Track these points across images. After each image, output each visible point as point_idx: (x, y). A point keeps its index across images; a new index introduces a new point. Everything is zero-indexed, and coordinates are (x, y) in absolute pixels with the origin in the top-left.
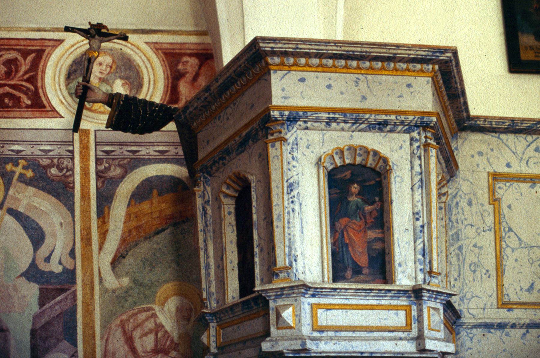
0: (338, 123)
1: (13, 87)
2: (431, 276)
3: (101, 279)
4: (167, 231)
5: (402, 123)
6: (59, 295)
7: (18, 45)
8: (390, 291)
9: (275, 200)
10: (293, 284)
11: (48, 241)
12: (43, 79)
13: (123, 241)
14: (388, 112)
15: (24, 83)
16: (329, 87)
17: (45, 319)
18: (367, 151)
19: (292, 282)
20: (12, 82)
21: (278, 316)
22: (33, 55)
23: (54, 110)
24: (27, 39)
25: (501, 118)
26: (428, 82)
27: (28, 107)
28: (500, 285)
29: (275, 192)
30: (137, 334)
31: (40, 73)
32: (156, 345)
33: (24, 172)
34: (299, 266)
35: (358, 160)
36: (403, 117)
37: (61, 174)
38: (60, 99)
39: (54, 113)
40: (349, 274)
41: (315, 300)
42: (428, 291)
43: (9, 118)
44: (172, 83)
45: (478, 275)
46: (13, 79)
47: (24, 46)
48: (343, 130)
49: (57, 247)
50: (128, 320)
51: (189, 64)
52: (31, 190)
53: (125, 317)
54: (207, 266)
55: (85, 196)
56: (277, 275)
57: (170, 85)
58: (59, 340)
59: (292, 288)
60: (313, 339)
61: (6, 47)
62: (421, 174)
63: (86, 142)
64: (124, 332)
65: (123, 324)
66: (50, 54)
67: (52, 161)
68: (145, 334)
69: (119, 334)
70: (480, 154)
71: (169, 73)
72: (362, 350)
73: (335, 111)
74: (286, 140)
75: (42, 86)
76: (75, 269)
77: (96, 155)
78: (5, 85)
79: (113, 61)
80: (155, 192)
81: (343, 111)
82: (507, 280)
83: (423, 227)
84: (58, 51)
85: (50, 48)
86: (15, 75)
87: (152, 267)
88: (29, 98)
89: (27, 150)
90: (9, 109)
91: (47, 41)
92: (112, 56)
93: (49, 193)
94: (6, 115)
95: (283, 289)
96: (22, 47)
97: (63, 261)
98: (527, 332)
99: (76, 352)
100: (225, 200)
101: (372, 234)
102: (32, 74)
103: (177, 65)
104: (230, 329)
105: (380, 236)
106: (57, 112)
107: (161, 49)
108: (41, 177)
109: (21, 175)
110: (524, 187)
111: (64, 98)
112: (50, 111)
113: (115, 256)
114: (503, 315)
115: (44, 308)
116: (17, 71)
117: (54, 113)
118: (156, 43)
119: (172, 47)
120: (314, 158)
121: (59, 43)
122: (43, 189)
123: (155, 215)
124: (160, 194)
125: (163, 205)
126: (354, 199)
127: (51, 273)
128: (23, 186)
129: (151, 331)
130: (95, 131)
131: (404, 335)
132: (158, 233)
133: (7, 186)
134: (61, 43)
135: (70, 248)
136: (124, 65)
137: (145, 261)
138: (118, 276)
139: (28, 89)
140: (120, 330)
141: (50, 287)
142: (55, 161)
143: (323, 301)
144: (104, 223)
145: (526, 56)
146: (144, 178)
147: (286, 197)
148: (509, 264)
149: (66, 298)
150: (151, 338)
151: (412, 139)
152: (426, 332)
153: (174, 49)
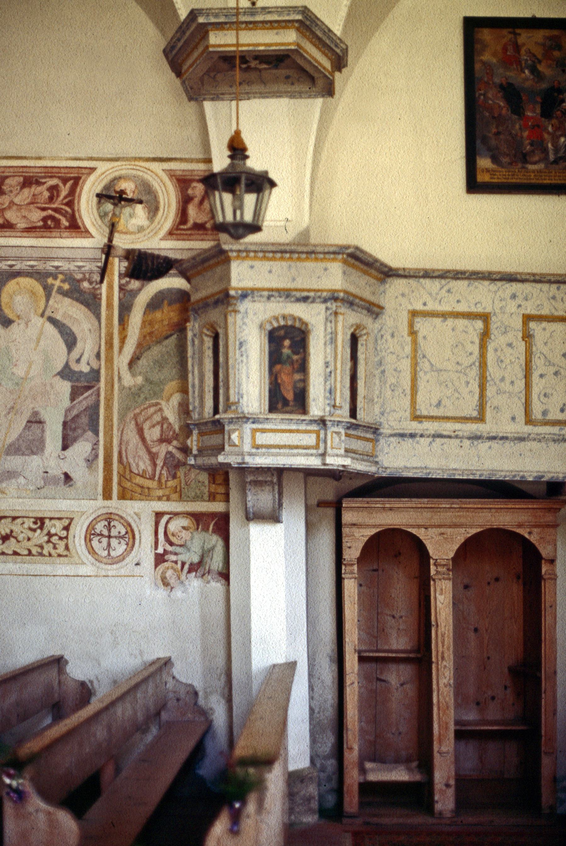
0: (275, 298)
1: (56, 210)
2: (334, 409)
3: (120, 378)
4: (175, 336)
5: (319, 297)
6: (87, 391)
8: (304, 420)
9: (231, 354)
10: (239, 416)
11: (79, 345)
13: (140, 345)
14: (309, 290)
15: (63, 207)
16: (270, 272)
17: (75, 412)
18: (294, 319)
19: (238, 413)
21: (229, 438)
22: (71, 182)
23: (87, 231)
24: (67, 167)
25: (417, 269)
26: (339, 266)
27: (66, 228)
28: (413, 402)
29: (231, 349)
30: (146, 426)
31: (77, 198)
32: (161, 435)
33: (62, 285)
34: (244, 401)
35: (290, 323)
36: (319, 294)
37: (91, 287)
39: (87, 233)
40: (280, 406)
41: (255, 426)
42: (330, 421)
44: (183, 206)
45: (397, 393)
46: (54, 203)
47: (65, 173)
48: (279, 302)
49: (86, 350)
50: (141, 413)
51: (198, 189)
52: (67, 301)
53: (137, 411)
54: (193, 386)
55: (110, 306)
56: (230, 407)
57: (181, 208)
58: (85, 431)
59: (238, 418)
60: (250, 454)
61: (50, 175)
62: (331, 333)
64: (137, 424)
65: (135, 417)
66: (84, 181)
67: (85, 276)
68: (154, 426)
69: (132, 425)
70: (403, 295)
72: (285, 463)
73: (272, 290)
74: (239, 311)
75: (78, 210)
76: (100, 369)
77: (119, 271)
78: (48, 209)
79: (136, 186)
80: (166, 302)
81: (278, 290)
82: (420, 398)
83: (331, 372)
84: (92, 178)
86: (57, 199)
87: (161, 367)
88: (67, 220)
89: (65, 266)
92: (135, 182)
93: (82, 303)
94: (48, 234)
95: (232, 418)
96: (63, 175)
97: (90, 362)
98: (433, 441)
99: (98, 441)
100: (206, 339)
101: (297, 377)
103: (187, 190)
104: (206, 437)
105: (302, 377)
107: (174, 176)
108: (75, 289)
109: (60, 288)
110: (437, 321)
113: (132, 357)
114: (415, 426)
115: (75, 402)
116: (58, 196)
117: (87, 233)
118: (171, 170)
119: (184, 173)
120: (258, 321)
122: (77, 300)
123: (166, 323)
124: (170, 304)
125: (172, 314)
126: (286, 351)
127: (81, 372)
128: (60, 297)
129: (158, 423)
131: (314, 451)
132: (167, 338)
133: (48, 297)
134: (94, 171)
135: (96, 351)
136: (145, 190)
137: (156, 362)
138: (134, 375)
139: (66, 212)
140: (133, 422)
141: (80, 385)
142: (87, 276)
143: (260, 426)
144: (124, 329)
145: (482, 178)
146: (158, 291)
147: (237, 351)
148: (422, 385)
149: (92, 394)
150: (157, 429)
151: (327, 309)
152: (329, 450)
153: (185, 176)
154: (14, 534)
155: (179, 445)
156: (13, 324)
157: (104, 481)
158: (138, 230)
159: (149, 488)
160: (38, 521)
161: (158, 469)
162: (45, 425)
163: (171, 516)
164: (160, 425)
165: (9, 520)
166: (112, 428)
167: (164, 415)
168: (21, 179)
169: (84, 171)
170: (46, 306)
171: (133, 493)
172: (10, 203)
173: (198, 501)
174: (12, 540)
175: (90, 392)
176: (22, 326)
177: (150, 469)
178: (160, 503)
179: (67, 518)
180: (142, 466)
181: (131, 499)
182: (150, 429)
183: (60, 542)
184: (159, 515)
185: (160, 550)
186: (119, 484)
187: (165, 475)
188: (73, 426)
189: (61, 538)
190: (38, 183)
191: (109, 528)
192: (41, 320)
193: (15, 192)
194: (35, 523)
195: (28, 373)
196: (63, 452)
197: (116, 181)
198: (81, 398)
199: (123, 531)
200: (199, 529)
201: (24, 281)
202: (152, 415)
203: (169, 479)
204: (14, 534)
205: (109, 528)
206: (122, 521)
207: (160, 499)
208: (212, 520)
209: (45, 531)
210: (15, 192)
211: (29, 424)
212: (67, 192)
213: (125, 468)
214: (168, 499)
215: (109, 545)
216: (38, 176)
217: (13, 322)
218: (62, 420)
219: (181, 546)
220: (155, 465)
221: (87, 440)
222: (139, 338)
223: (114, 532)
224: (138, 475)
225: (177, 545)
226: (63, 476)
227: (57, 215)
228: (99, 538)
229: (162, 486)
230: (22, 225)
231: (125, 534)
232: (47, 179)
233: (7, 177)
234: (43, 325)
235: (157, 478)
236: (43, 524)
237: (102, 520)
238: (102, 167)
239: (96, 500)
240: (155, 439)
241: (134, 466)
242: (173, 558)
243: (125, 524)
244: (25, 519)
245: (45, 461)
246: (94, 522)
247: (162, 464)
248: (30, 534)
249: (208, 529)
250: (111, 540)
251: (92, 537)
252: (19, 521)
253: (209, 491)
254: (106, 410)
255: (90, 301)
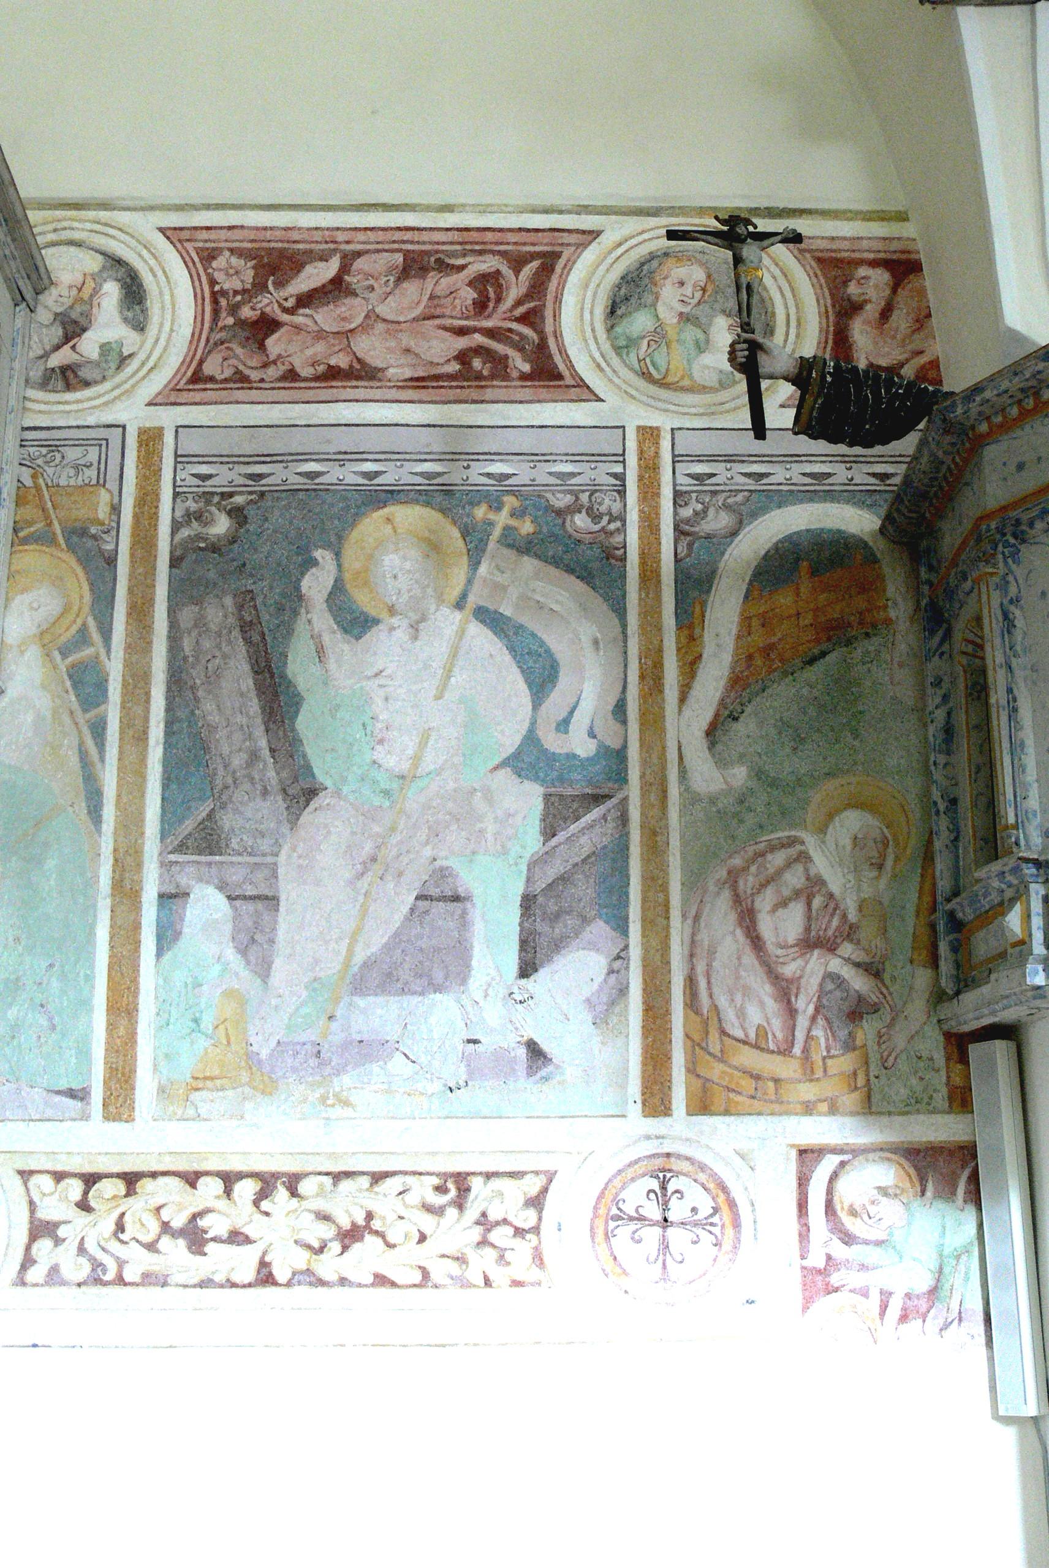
1: (491, 333)
3: (683, 773)
7: (501, 243)
11: (565, 680)
12: (556, 316)
13: (736, 682)
17: (552, 872)
20: (489, 324)
22: (535, 264)
23: (581, 384)
27: (524, 377)
30: (764, 903)
32: (808, 929)
33: (513, 522)
37: (597, 528)
38: (594, 360)
43: (482, 402)
44: (837, 324)
50: (745, 869)
52: (529, 564)
57: (832, 329)
58: (585, 920)
63: (652, 454)
64: (737, 899)
65: (733, 877)
68: (783, 903)
71: (829, 301)
76: (625, 746)
79: (709, 277)
84: (589, 255)
85: (573, 248)
89: (522, 473)
90: (483, 383)
91: (565, 234)
93: (570, 570)
94: (474, 394)
97: (596, 730)
102: (532, 305)
103: (845, 283)
106: (588, 387)
111: (603, 356)
112: (574, 386)
116: (499, 300)
121: (590, 238)
129: (797, 894)
130: (672, 429)
133: (475, 555)
135: (612, 700)
138: (722, 763)
139: (523, 337)
140: (727, 894)
141: (569, 791)
142: (584, 498)
144: (692, 638)
149: (604, 817)
150: (795, 914)
154: (376, 1224)
155: (859, 956)
156: (375, 629)
157: (644, 1064)
158: (720, 382)
159: (776, 1081)
160: (451, 1185)
161: (802, 1023)
162: (469, 905)
163: (845, 1157)
164: (803, 899)
165: (365, 1181)
166: (667, 911)
167: (812, 873)
168: (399, 258)
169: (566, 238)
170: (470, 582)
171: (732, 1095)
172: (367, 317)
173: (918, 1112)
174: (368, 1238)
175: (596, 813)
176: (402, 635)
177: (777, 1026)
178: (807, 1120)
179: (537, 1173)
180: (755, 1016)
181: (727, 1112)
182: (774, 910)
183: (517, 1243)
184: (808, 1155)
185: (816, 1260)
186: (692, 1070)
187: (822, 1041)
188: (552, 907)
189: (519, 1232)
190: (444, 267)
191: (663, 1195)
192: (458, 616)
193: (379, 290)
194: (441, 1189)
195: (417, 759)
196: (524, 981)
197: (655, 263)
198: (574, 828)
199: (705, 1206)
200: (929, 1194)
201: (408, 515)
202: (780, 872)
203: (833, 1052)
204: (376, 1224)
205: (663, 1195)
206: (702, 1177)
207: (808, 1109)
208: (963, 1167)
209: (472, 1213)
210: (379, 290)
211: (423, 905)
212: (523, 290)
213: (706, 1023)
214: (833, 1110)
215: (665, 1246)
216: (443, 252)
217: (376, 622)
218: (517, 888)
219: (879, 1243)
220: (792, 1013)
221: (593, 946)
222: (735, 663)
223: (678, 1211)
224: (745, 1043)
225: (866, 1242)
226: (522, 1052)
227: (500, 348)
228: (633, 1226)
229: (812, 1071)
230: (399, 370)
231: (712, 1215)
232: (469, 259)
233: (359, 254)
234: (461, 633)
235: (797, 1050)
236: (464, 1190)
237: (644, 1175)
238: (614, 230)
239: (624, 1116)
240: (791, 941)
241: (730, 1016)
242: (856, 1279)
243: (711, 1186)
244: (410, 1180)
245: (469, 1009)
246: (617, 1183)
247: (811, 1009)
248: (427, 1222)
249: (954, 1193)
250: (671, 1232)
251: (612, 1224)
252: (392, 1185)
253: (947, 1084)
254: (646, 861)
255: (596, 565)
